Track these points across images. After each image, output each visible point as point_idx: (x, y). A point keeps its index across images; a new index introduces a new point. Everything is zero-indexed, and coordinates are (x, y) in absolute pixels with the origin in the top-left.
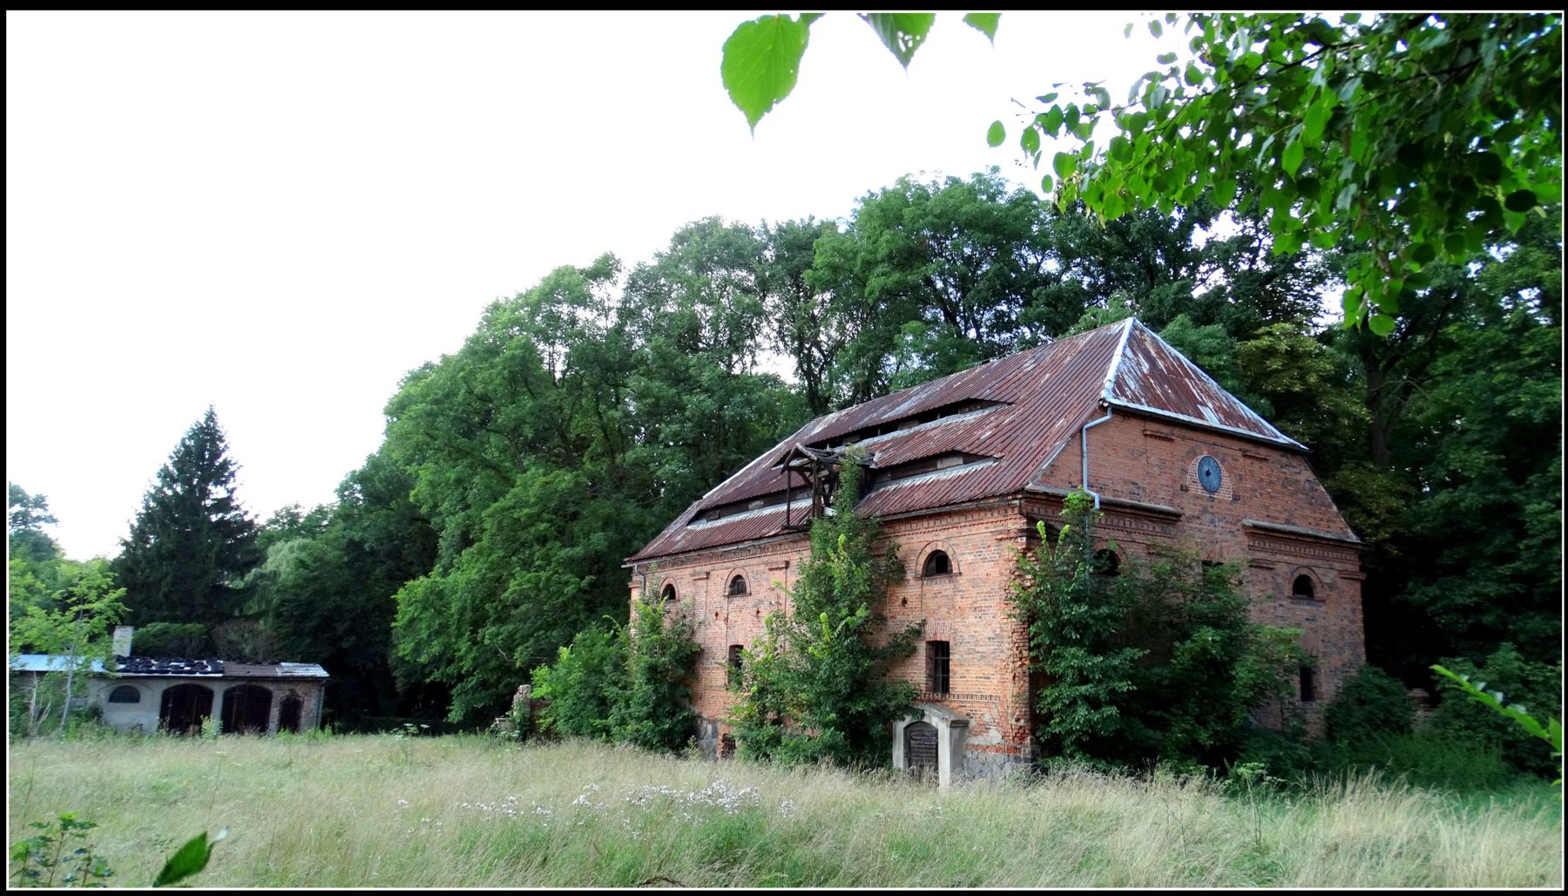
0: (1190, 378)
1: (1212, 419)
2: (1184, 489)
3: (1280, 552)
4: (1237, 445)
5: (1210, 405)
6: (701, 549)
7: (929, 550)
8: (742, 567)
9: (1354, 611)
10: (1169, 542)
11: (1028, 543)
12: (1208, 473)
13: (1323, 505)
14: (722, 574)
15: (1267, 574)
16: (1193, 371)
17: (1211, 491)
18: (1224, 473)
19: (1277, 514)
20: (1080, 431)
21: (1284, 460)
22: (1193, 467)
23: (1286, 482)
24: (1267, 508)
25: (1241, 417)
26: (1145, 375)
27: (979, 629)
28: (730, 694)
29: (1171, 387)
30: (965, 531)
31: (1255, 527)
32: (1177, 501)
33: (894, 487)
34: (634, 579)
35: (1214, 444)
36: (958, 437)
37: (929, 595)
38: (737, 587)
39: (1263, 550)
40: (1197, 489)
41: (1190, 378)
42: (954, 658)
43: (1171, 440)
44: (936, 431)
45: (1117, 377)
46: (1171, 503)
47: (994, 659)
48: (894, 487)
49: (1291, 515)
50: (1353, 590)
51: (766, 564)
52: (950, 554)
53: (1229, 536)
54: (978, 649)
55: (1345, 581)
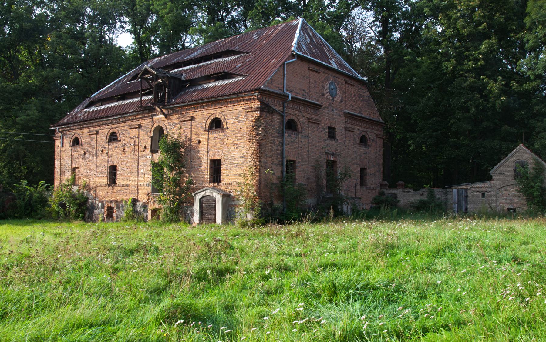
0: (326, 48)
1: (335, 66)
2: (323, 95)
3: (357, 125)
4: (343, 78)
5: (333, 59)
6: (93, 119)
7: (212, 118)
8: (116, 128)
9: (380, 150)
10: (317, 118)
11: (260, 114)
12: (332, 89)
13: (372, 107)
14: (105, 131)
15: (351, 134)
16: (327, 45)
17: (333, 97)
18: (338, 90)
19: (356, 109)
20: (284, 64)
21: (360, 87)
22: (327, 86)
23: (360, 96)
24: (353, 106)
25: (345, 66)
26: (309, 44)
27: (236, 153)
28: (110, 188)
29: (318, 50)
30: (230, 108)
31: (349, 113)
32: (320, 99)
33: (193, 89)
34: (56, 135)
35: (335, 77)
36: (225, 66)
37: (212, 138)
38: (113, 138)
39: (351, 124)
40: (327, 95)
41: (326, 48)
42: (223, 167)
43: (319, 73)
44: (212, 65)
45: (298, 42)
46: (318, 101)
47: (243, 166)
48: (193, 89)
49: (361, 110)
50: (380, 142)
51: (128, 126)
52: (222, 119)
53: (338, 117)
54: (235, 162)
55: (378, 138)
